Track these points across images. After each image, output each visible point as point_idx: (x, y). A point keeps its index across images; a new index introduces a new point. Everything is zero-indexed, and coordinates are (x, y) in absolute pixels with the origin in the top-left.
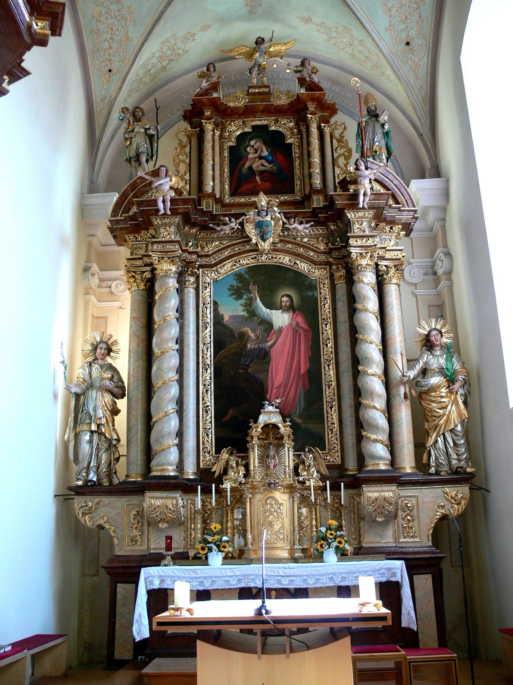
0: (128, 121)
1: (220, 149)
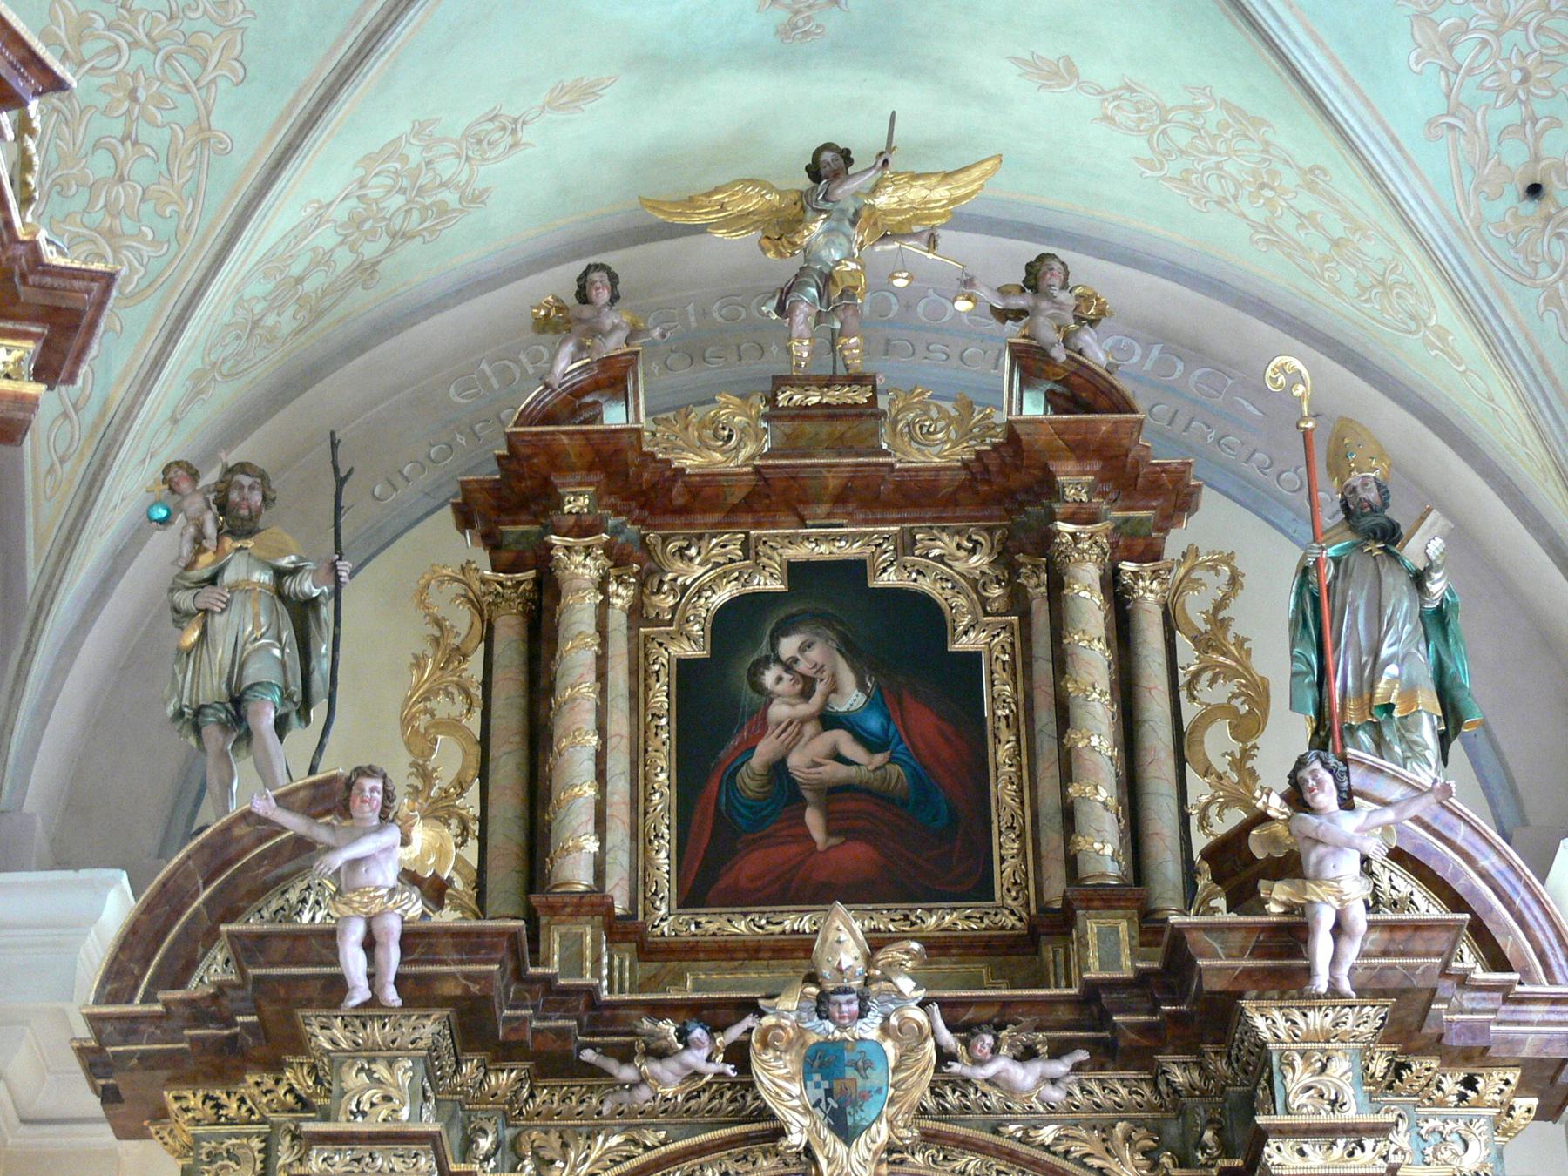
0: (192, 530)
1: (633, 672)
